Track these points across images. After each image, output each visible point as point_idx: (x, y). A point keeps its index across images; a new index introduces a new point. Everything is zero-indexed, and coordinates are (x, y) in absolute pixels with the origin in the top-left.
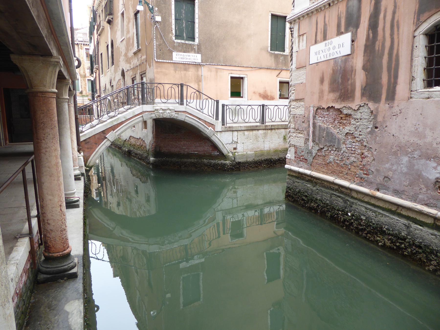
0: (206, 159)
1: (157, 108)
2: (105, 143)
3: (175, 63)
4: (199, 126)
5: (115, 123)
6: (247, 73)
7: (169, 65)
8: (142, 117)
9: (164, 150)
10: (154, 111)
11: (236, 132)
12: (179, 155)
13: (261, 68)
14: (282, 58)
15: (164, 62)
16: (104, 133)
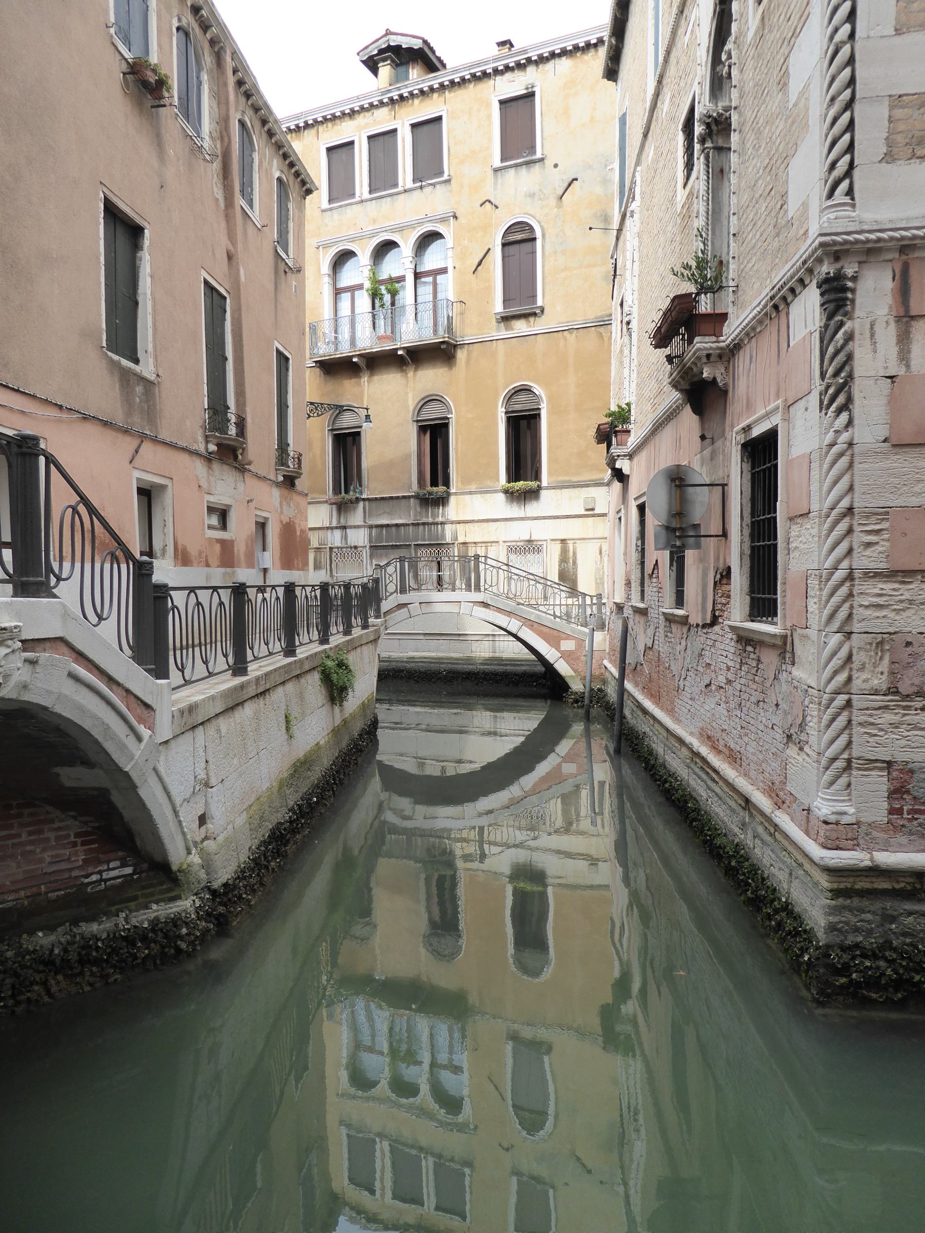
4: (107, 728)
13: (86, 418)
14: (139, 389)
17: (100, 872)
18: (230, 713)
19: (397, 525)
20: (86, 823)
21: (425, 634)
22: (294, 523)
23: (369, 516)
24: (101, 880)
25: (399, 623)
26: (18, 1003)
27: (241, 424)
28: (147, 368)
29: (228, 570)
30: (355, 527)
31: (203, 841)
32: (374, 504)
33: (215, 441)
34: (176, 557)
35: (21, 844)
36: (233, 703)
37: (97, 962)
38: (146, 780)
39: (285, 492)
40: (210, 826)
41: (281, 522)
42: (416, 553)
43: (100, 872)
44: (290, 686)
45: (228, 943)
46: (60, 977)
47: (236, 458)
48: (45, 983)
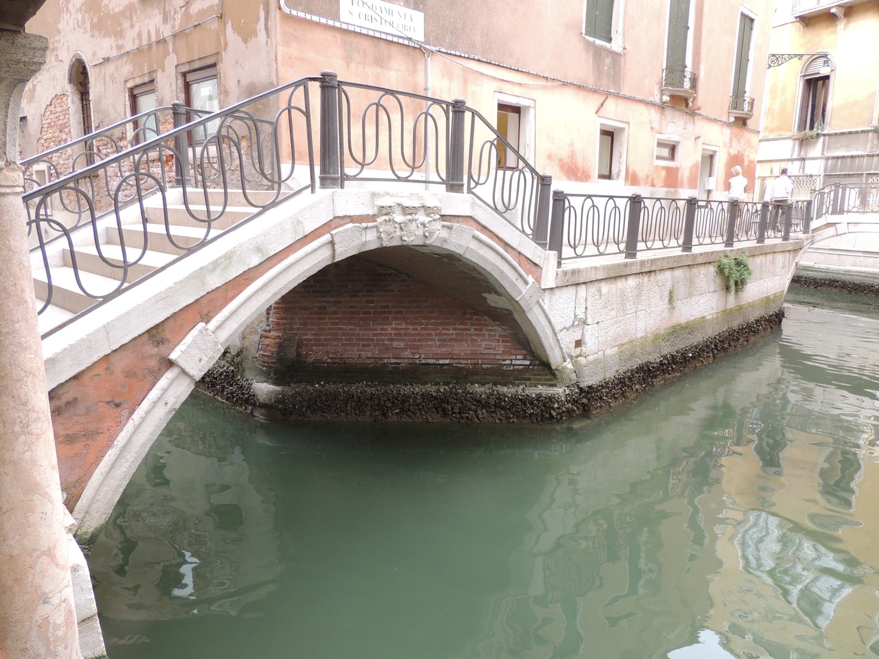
0: (483, 384)
1: (386, 202)
2: (165, 391)
3: (347, 31)
4: (502, 272)
5: (215, 281)
6: (535, 94)
7: (328, 36)
8: (332, 243)
9: (317, 354)
10: (373, 218)
11: (584, 286)
12: (377, 373)
13: (565, 84)
14: (608, 61)
15: (311, 23)
16: (158, 335)
17: (511, 360)
18: (613, 281)
19: (852, 157)
20: (505, 330)
21: (864, 252)
22: (743, 155)
23: (828, 149)
24: (511, 364)
25: (826, 240)
26: (462, 418)
27: (694, 81)
28: (616, 45)
29: (672, 190)
30: (813, 159)
31: (577, 357)
32: (833, 139)
33: (669, 93)
34: (626, 178)
35: (471, 335)
36: (615, 275)
37: (503, 408)
38: (531, 309)
39: (736, 130)
40: (583, 348)
41: (729, 154)
42: (867, 180)
43: (511, 360)
44: (679, 273)
45: (586, 423)
46: (484, 411)
47: (687, 105)
48: (476, 411)
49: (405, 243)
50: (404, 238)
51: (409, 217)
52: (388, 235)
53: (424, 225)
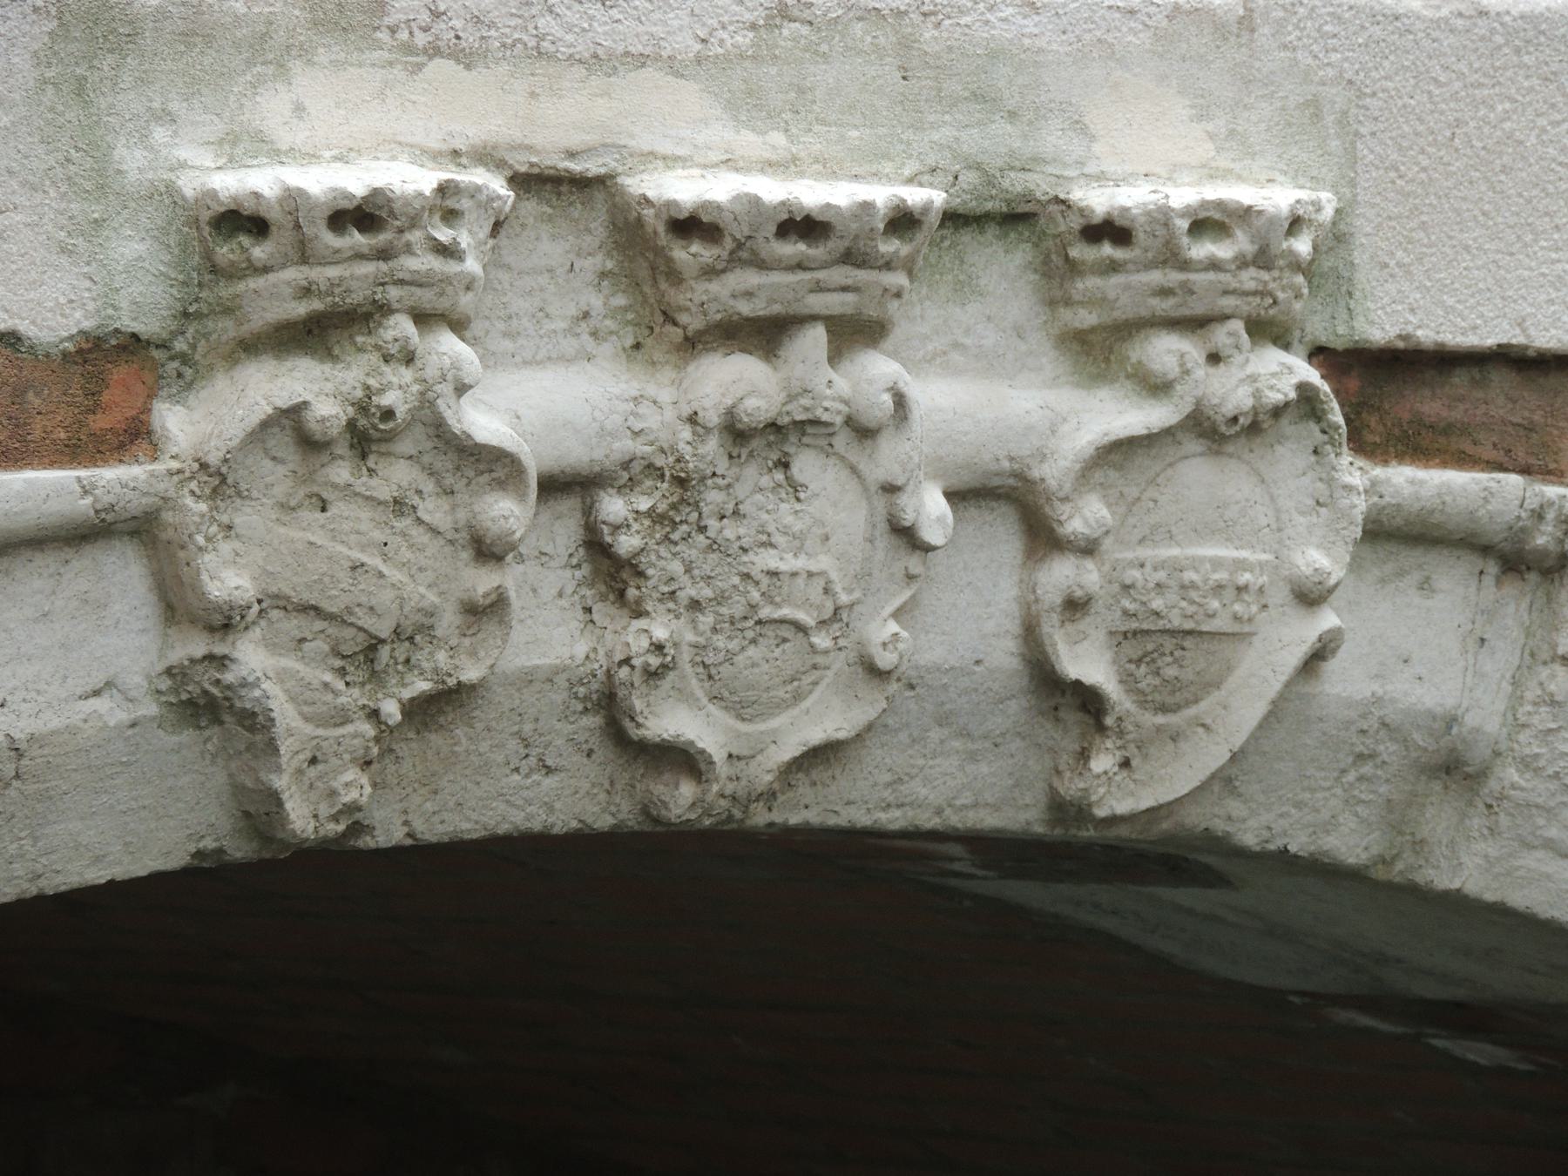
49: (680, 799)
50: (671, 719)
51: (735, 381)
52: (366, 657)
53: (1011, 500)
